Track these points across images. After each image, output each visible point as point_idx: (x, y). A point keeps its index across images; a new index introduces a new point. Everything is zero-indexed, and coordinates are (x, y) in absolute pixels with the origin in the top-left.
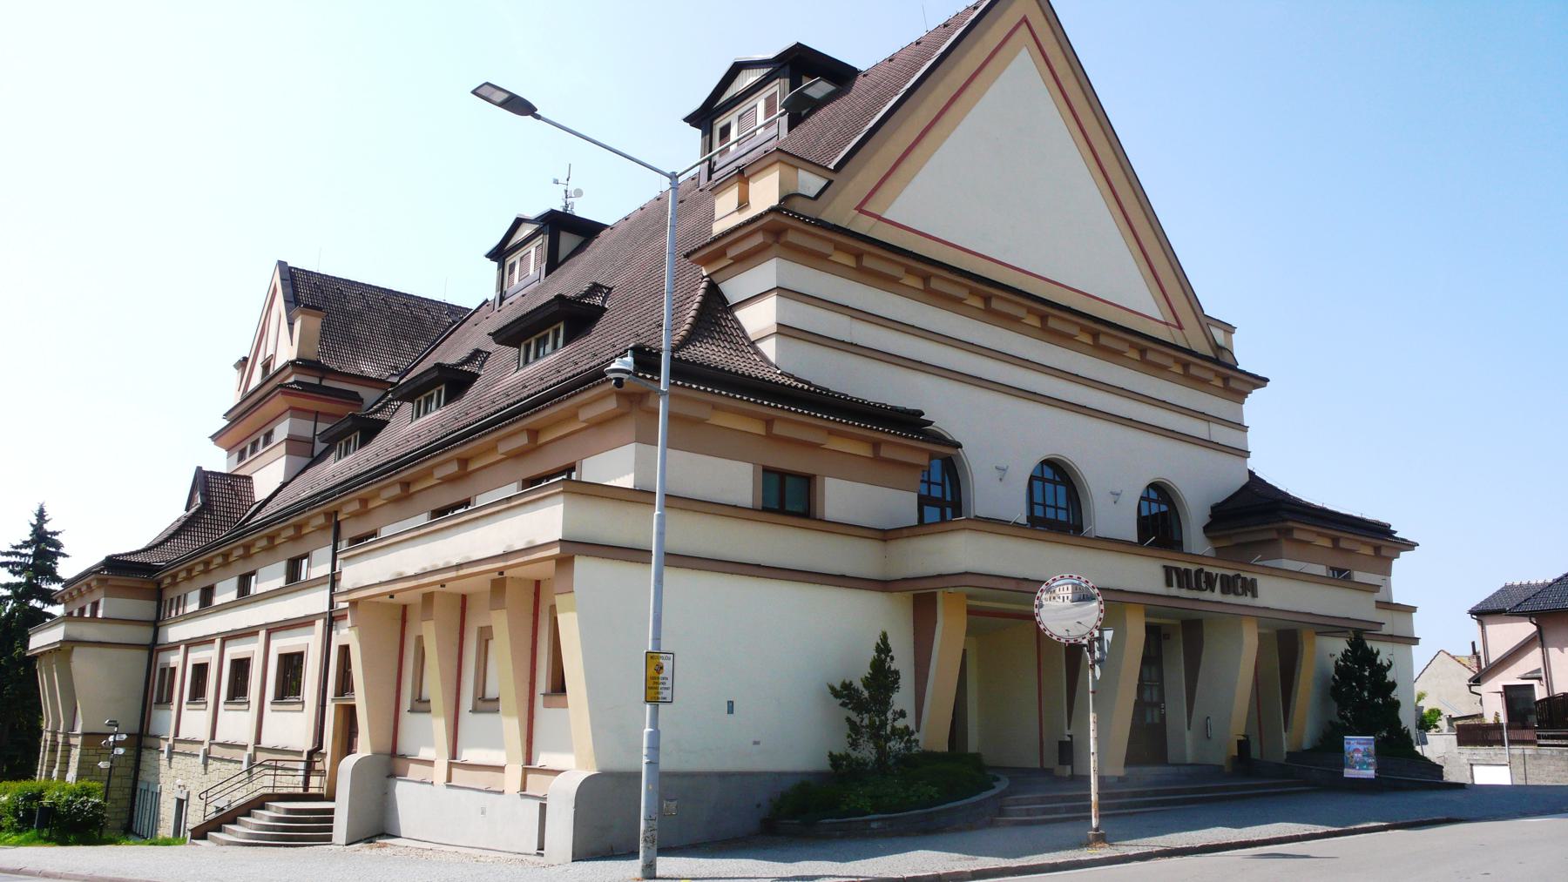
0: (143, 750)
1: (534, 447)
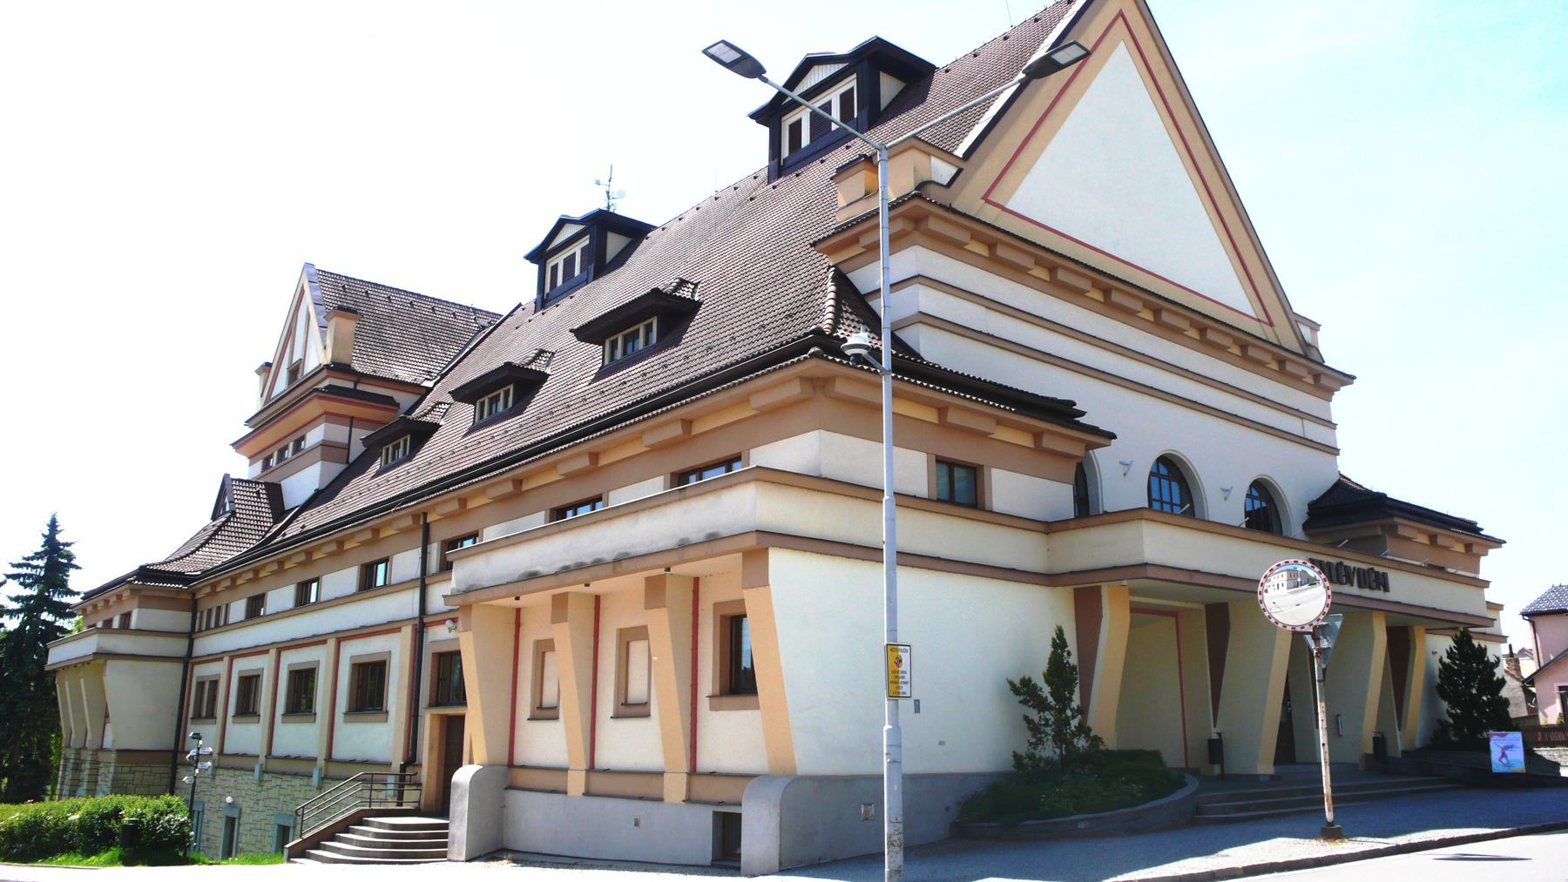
0: (179, 767)
1: (688, 437)
